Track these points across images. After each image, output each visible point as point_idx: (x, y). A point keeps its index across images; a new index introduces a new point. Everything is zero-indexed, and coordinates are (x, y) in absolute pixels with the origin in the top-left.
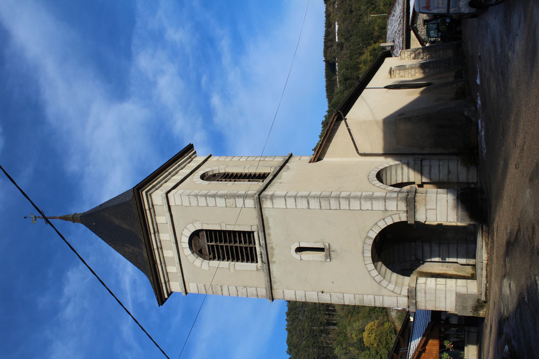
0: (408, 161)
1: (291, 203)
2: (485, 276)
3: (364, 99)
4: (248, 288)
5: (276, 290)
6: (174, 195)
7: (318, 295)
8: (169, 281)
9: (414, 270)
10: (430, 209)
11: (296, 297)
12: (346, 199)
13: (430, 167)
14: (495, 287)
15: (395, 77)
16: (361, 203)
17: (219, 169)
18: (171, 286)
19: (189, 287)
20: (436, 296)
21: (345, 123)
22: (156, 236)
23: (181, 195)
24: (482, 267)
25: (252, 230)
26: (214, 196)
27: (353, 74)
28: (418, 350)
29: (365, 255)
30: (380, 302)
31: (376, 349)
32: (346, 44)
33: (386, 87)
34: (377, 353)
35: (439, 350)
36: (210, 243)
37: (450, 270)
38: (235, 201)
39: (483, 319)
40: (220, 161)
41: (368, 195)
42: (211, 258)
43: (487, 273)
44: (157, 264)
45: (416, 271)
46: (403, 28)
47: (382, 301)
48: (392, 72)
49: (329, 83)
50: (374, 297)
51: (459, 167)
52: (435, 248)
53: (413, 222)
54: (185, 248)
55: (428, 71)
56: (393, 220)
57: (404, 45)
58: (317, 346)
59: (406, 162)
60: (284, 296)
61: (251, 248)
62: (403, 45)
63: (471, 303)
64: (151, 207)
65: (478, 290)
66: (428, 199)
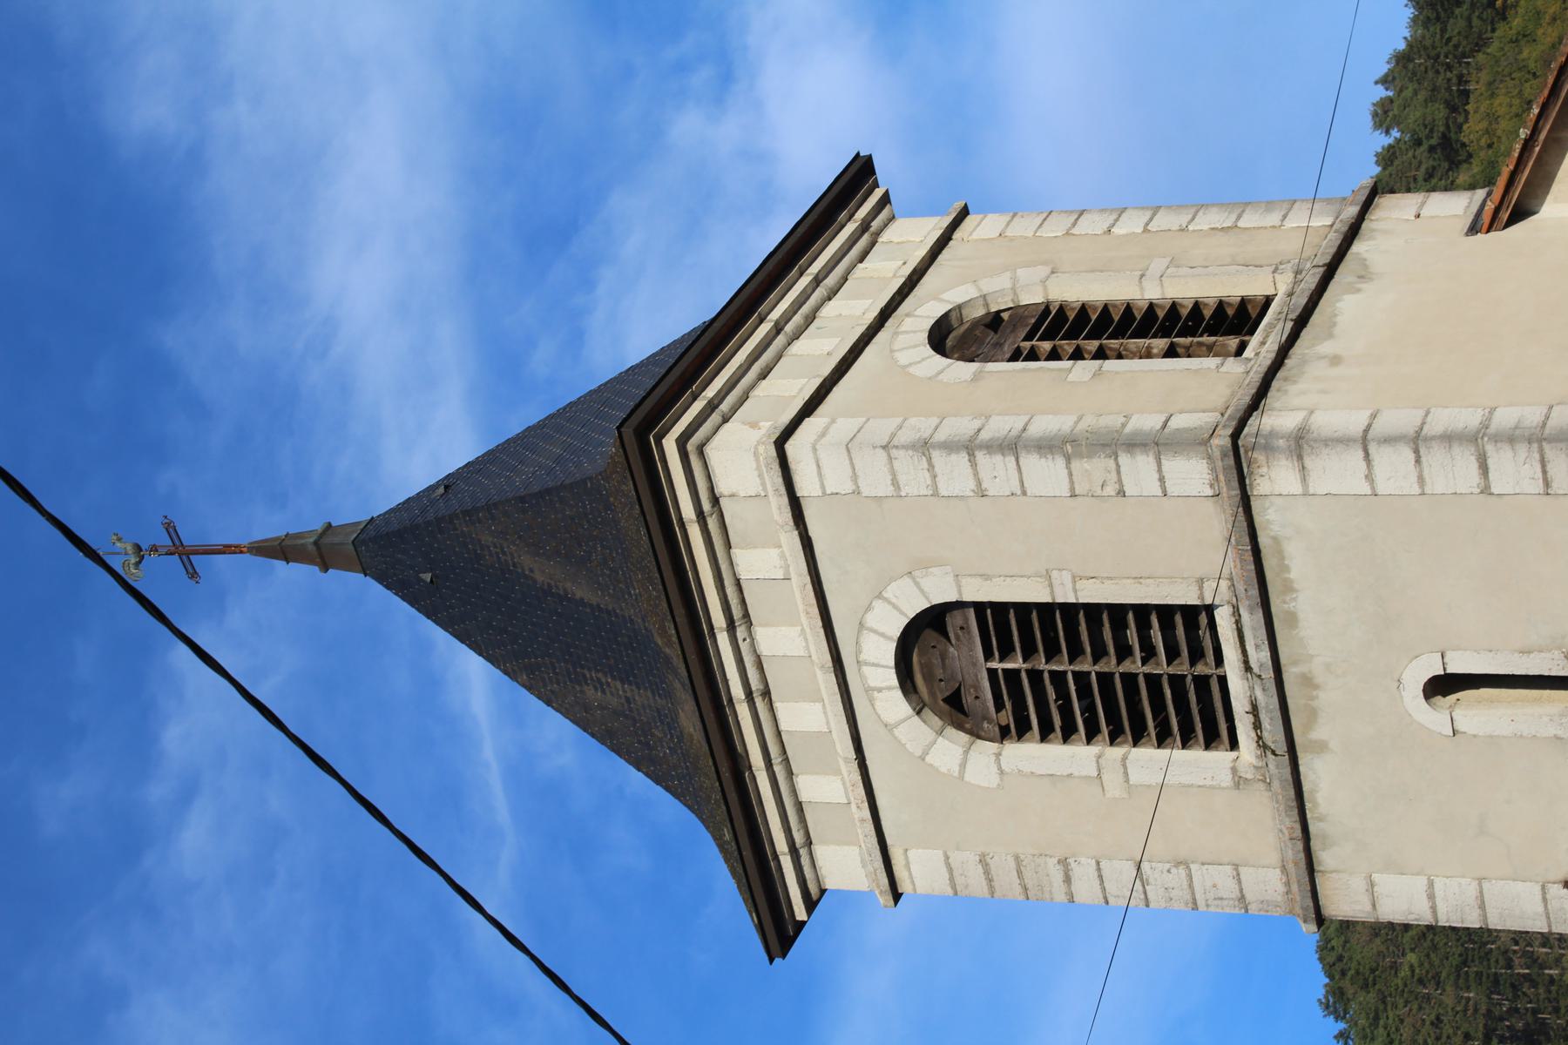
1: (1394, 469)
4: (1193, 867)
5: (1334, 875)
6: (815, 450)
7: (1545, 900)
8: (809, 843)
11: (1434, 909)
17: (1014, 289)
18: (820, 862)
19: (908, 865)
22: (740, 642)
25: (1203, 599)
26: (1012, 446)
36: (1001, 660)
38: (1118, 466)
40: (1012, 239)
42: (1003, 723)
54: (880, 690)
58: (1479, 975)
60: (1374, 906)
61: (1202, 682)
64: (706, 506)
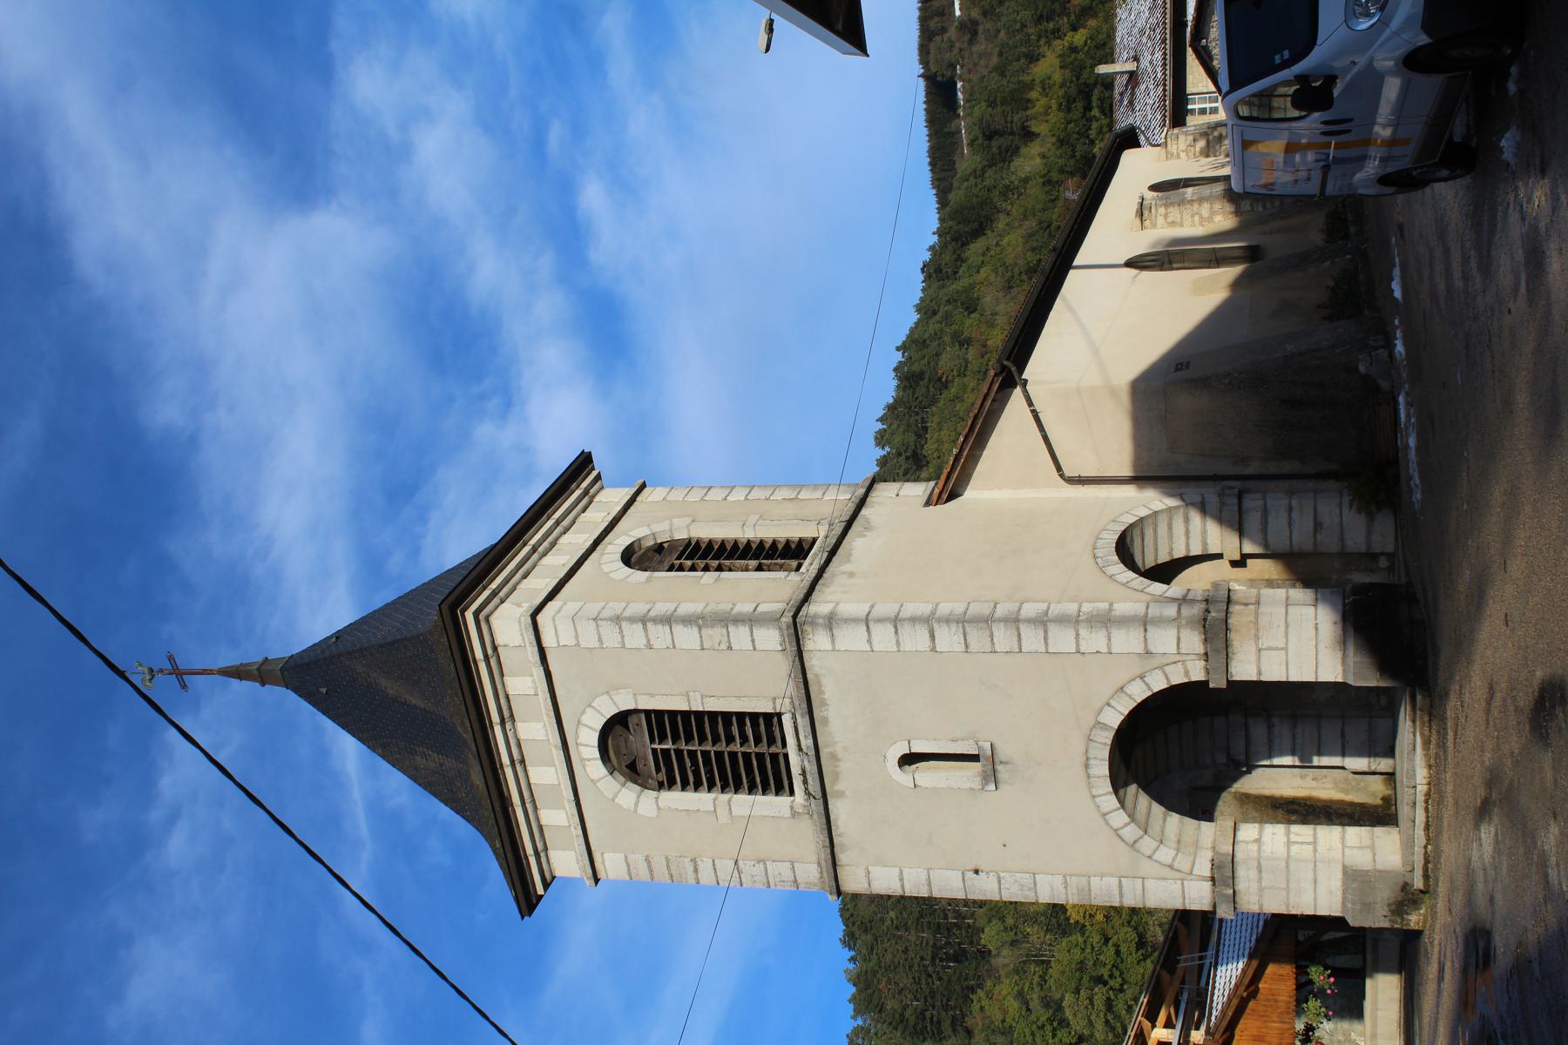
0: (1202, 496)
1: (883, 637)
2: (1423, 826)
3: (1071, 309)
5: (847, 868)
6: (554, 620)
7: (964, 880)
8: (546, 849)
9: (1223, 789)
10: (1270, 649)
13: (1265, 512)
14: (1450, 850)
15: (1154, 226)
17: (671, 530)
19: (603, 862)
20: (1288, 876)
21: (1025, 396)
22: (508, 731)
23: (573, 620)
24: (1413, 798)
26: (668, 620)
27: (1009, 119)
28: (1238, 993)
29: (1091, 772)
30: (1135, 894)
31: (1103, 929)
32: (985, 26)
33: (1130, 264)
34: (1107, 940)
35: (1295, 992)
36: (659, 744)
37: (1323, 789)
38: (728, 632)
39: (1417, 934)
40: (670, 502)
42: (660, 780)
43: (1427, 817)
44: (512, 805)
45: (1230, 793)
46: (1165, 23)
48: (1146, 213)
49: (938, 143)
50: (1120, 881)
51: (1346, 510)
52: (1283, 730)
53: (1223, 685)
54: (589, 760)
55: (1249, 209)
57: (1168, 72)
58: (929, 923)
59: (1198, 499)
61: (774, 757)
62: (1164, 73)
63: (1384, 895)
64: (490, 652)
65: (1402, 859)
66: (1263, 621)
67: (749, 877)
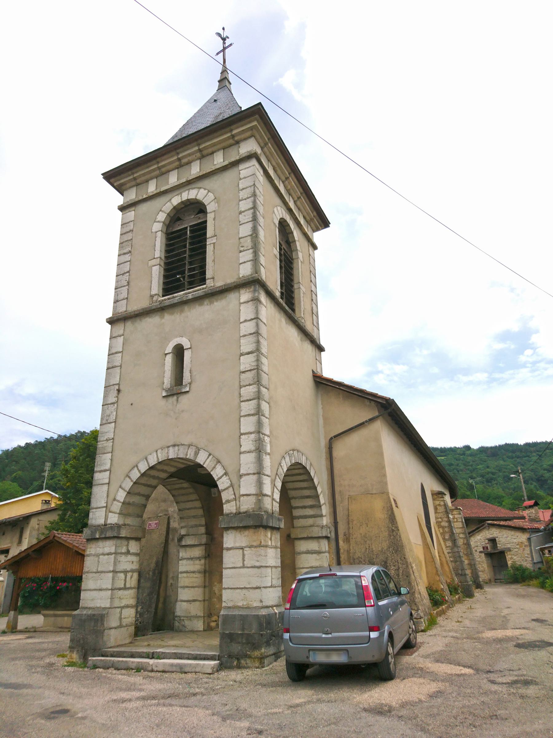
0: (325, 516)
1: (249, 327)
4: (127, 287)
7: (114, 385)
10: (244, 555)
12: (257, 410)
16: (251, 433)
26: (255, 219)
29: (171, 448)
38: (249, 250)
41: (265, 445)
47: (101, 483)
54: (181, 196)
56: (224, 490)
67: (120, 279)
